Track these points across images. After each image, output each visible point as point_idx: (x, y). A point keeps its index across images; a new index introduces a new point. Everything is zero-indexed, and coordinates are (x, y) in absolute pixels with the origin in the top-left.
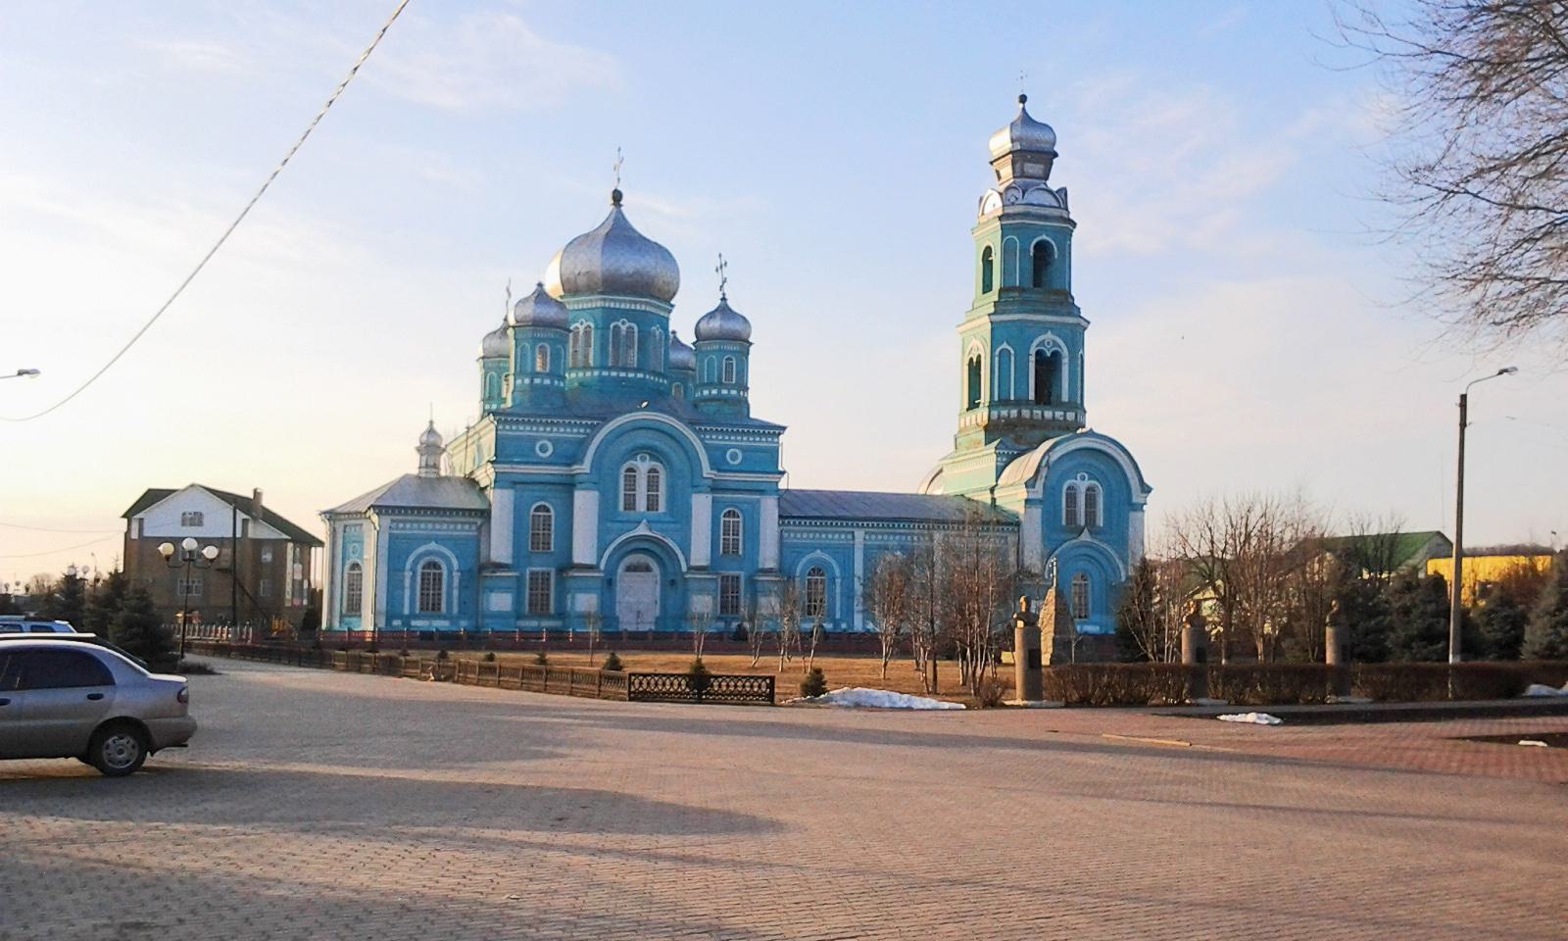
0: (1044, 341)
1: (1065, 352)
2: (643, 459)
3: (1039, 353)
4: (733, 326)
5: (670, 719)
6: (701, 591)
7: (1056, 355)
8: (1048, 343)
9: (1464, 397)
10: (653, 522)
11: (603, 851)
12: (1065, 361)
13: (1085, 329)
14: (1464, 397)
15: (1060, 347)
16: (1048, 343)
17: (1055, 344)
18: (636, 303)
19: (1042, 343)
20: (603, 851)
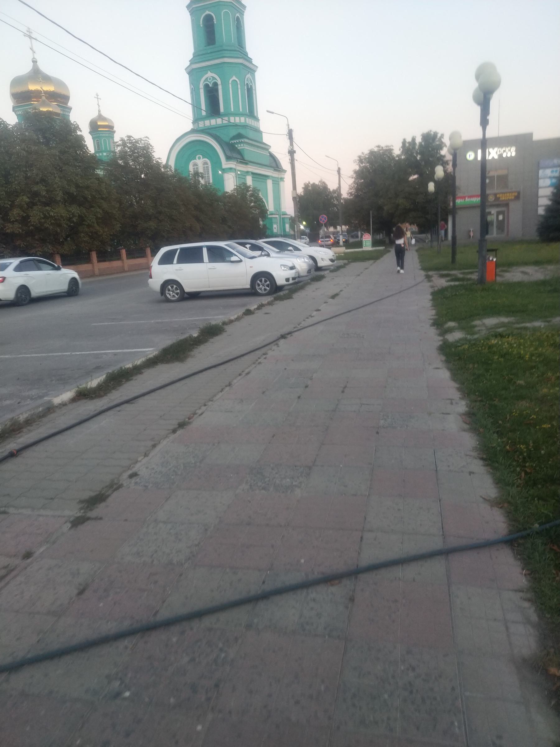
0: (207, 78)
1: (219, 82)
2: (199, 158)
3: (206, 86)
4: (110, 124)
5: (154, 356)
6: (287, 224)
7: (216, 84)
8: (210, 79)
9: (268, 111)
10: (273, 181)
11: (276, 184)
12: (220, 87)
13: (244, 12)
14: (268, 111)
15: (217, 80)
16: (210, 79)
17: (214, 78)
18: (96, 134)
19: (206, 80)
20: (276, 184)
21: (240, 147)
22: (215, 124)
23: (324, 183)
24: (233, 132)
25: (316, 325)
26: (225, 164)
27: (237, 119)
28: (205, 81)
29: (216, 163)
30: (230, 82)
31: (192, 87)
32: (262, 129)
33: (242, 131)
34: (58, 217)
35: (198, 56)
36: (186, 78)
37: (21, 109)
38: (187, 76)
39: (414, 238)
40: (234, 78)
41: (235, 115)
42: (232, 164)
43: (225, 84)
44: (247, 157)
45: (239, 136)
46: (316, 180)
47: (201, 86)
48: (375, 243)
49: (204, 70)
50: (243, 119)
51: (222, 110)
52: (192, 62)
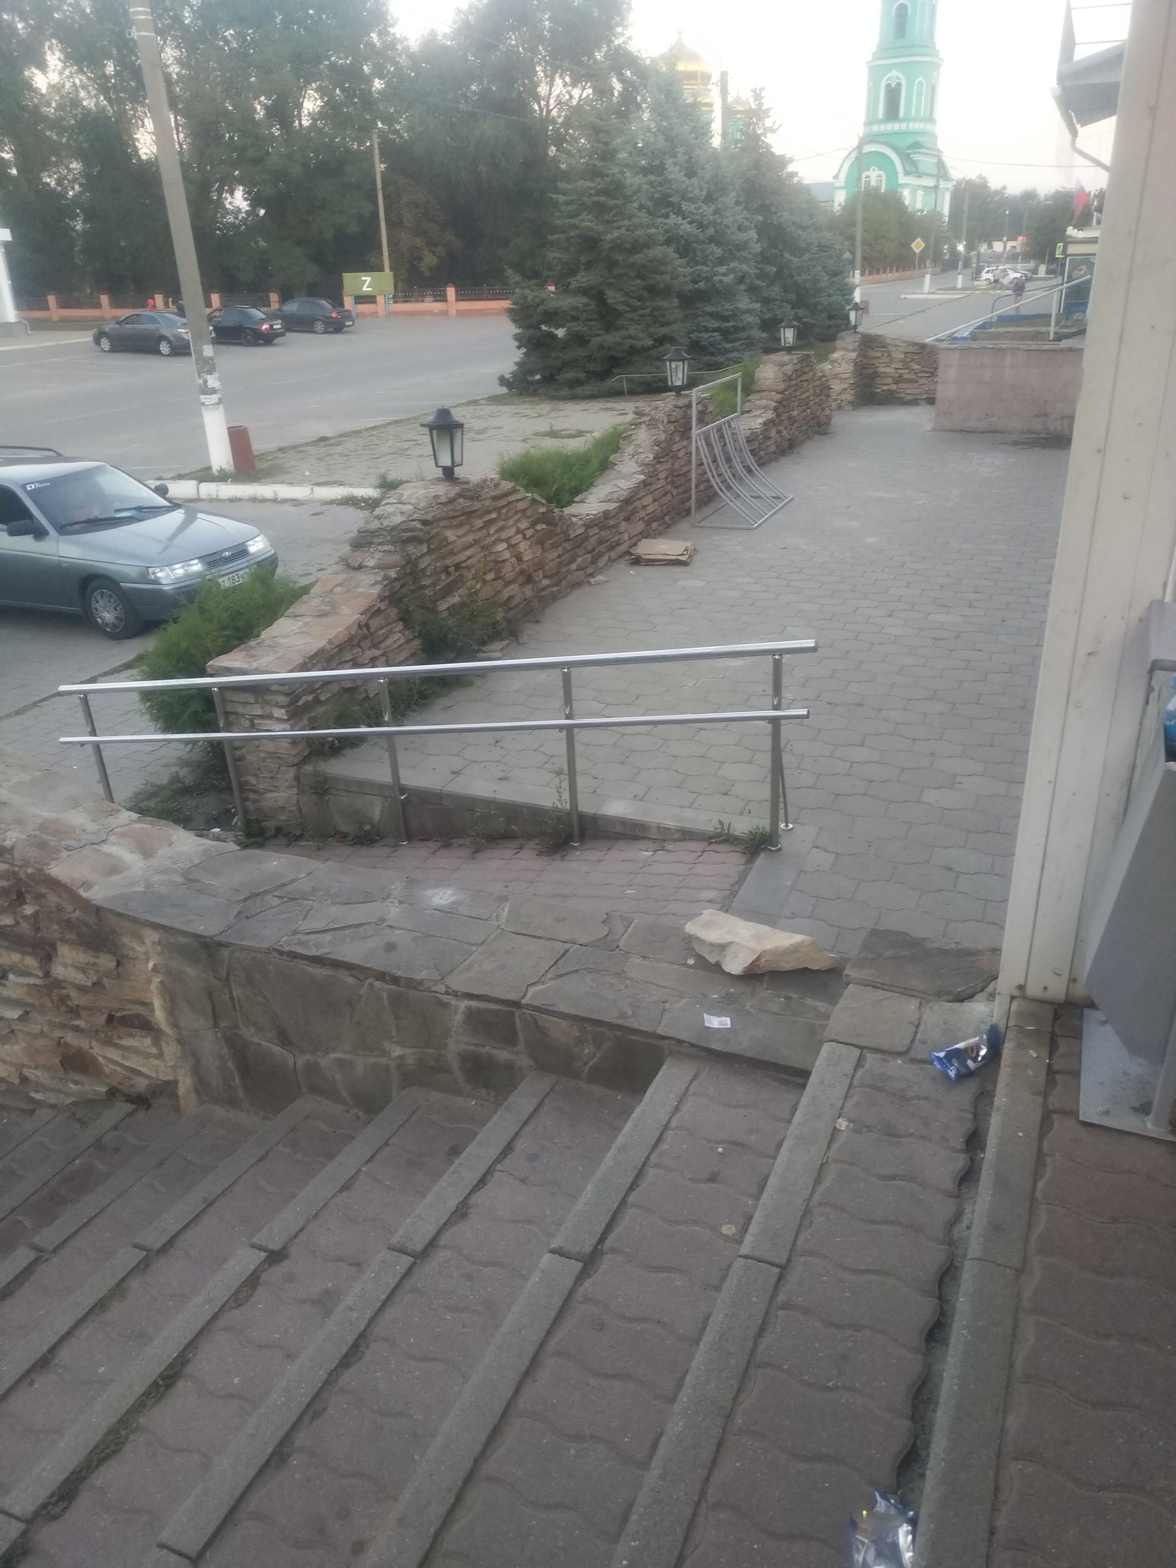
1: (904, 83)
3: (889, 85)
7: (899, 85)
12: (903, 90)
17: (898, 78)
21: (916, 157)
22: (898, 128)
23: (984, 178)
24: (910, 140)
25: (478, 1448)
26: (902, 179)
27: (917, 125)
28: (887, 80)
29: (892, 175)
30: (916, 82)
31: (871, 84)
32: (937, 133)
33: (921, 139)
34: (77, 187)
35: (884, 51)
36: (865, 73)
37: (1083, 279)
38: (867, 70)
39: (385, 83)
40: (920, 79)
41: (915, 120)
42: (910, 180)
43: (910, 86)
44: (922, 168)
45: (916, 145)
46: (972, 175)
47: (883, 85)
48: (1049, 272)
49: (890, 67)
50: (922, 125)
51: (901, 114)
52: (876, 56)
